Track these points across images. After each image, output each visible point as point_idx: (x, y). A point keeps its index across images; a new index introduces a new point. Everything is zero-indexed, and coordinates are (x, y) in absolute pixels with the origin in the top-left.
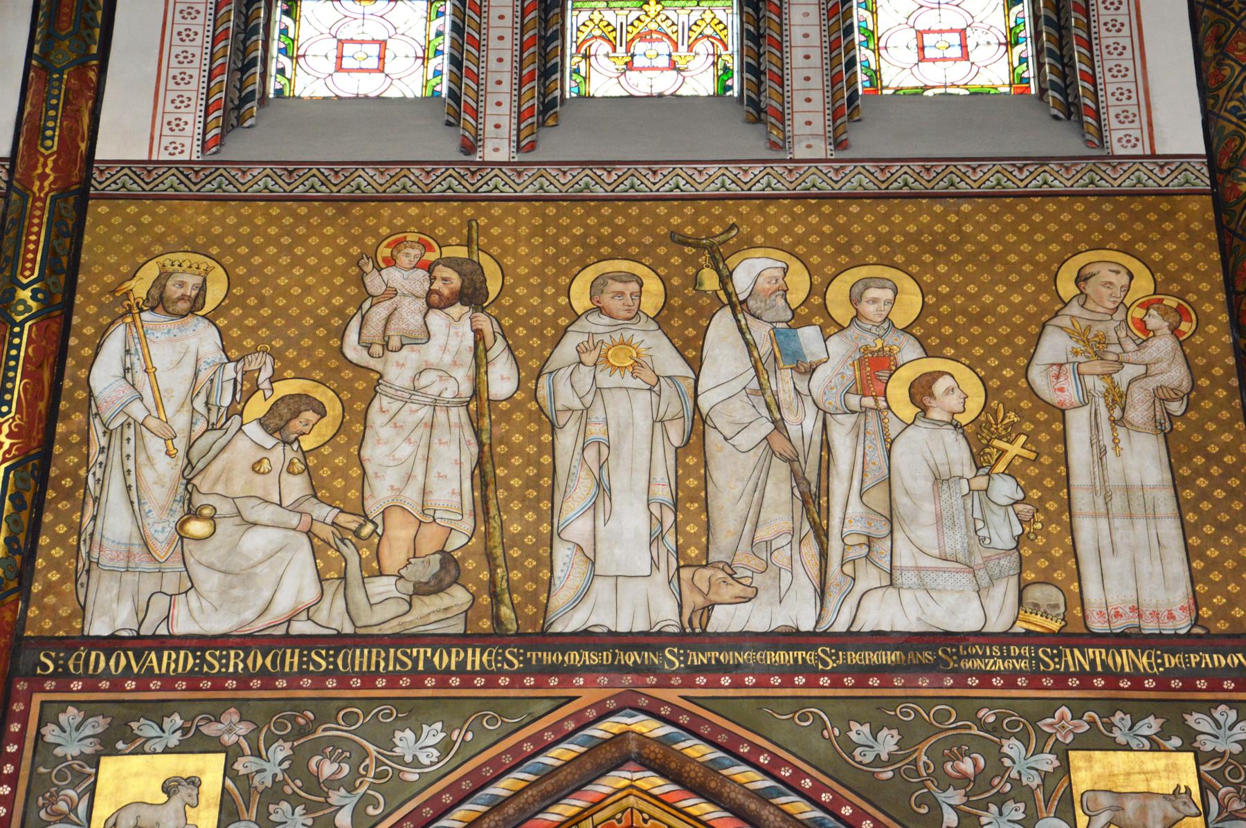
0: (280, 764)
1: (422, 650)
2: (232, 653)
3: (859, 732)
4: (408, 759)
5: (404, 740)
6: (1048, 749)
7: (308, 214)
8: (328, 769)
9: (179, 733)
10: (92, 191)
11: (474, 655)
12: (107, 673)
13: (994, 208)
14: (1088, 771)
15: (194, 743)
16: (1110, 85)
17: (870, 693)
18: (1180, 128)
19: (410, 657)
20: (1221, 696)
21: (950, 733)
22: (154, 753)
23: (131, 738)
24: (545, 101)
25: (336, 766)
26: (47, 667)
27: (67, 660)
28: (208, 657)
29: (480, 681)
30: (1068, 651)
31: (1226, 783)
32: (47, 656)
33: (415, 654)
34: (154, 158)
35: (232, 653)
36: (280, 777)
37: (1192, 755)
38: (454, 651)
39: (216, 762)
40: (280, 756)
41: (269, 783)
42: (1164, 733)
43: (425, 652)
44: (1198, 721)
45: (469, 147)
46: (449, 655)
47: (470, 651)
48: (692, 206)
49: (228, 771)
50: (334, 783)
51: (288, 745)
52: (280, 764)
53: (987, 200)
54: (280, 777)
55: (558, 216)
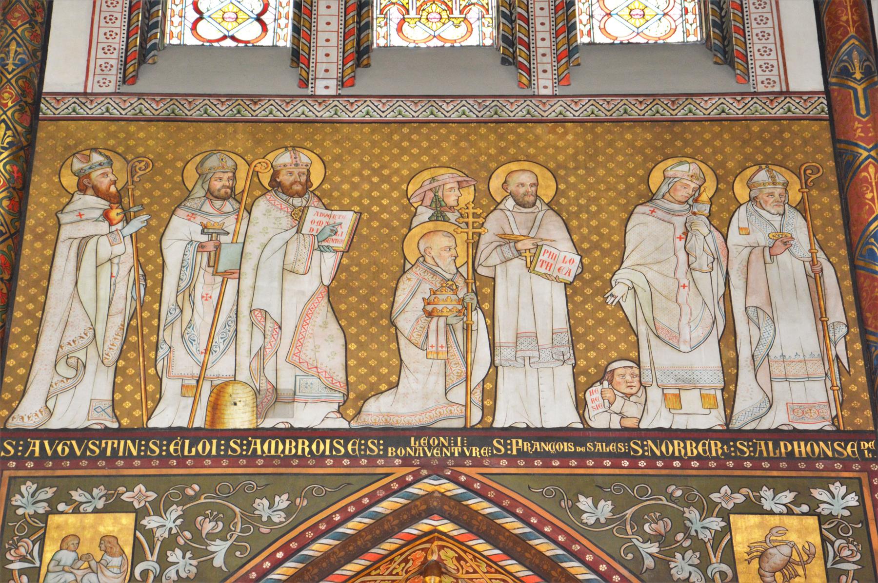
0: (174, 522)
1: (110, 442)
2: (514, 441)
3: (585, 503)
4: (265, 519)
5: (262, 506)
6: (715, 515)
7: (186, 134)
8: (208, 526)
9: (104, 499)
10: (41, 115)
11: (799, 447)
12: (347, 455)
13: (717, 129)
14: (747, 531)
15: (115, 506)
16: (756, 45)
17: (639, 472)
18: (807, 75)
19: (99, 447)
20: (833, 474)
21: (647, 503)
22: (86, 513)
23: (69, 501)
24: (359, 52)
25: (213, 524)
26: (638, 452)
27: (168, 446)
28: (232, 444)
29: (802, 465)
30: (762, 443)
31: (839, 537)
32: (9, 444)
33: (103, 445)
34: (89, 91)
35: (514, 441)
36: (174, 531)
37: (816, 517)
38: (288, 441)
39: (127, 520)
40: (174, 516)
41: (166, 535)
42: (796, 502)
43: (113, 443)
44: (819, 494)
45: (304, 83)
46: (284, 444)
47: (795, 443)
48: (581, 127)
49: (138, 526)
50: (212, 536)
51: (180, 508)
52: (174, 522)
53: (812, 122)
54: (174, 531)
55: (410, 134)
